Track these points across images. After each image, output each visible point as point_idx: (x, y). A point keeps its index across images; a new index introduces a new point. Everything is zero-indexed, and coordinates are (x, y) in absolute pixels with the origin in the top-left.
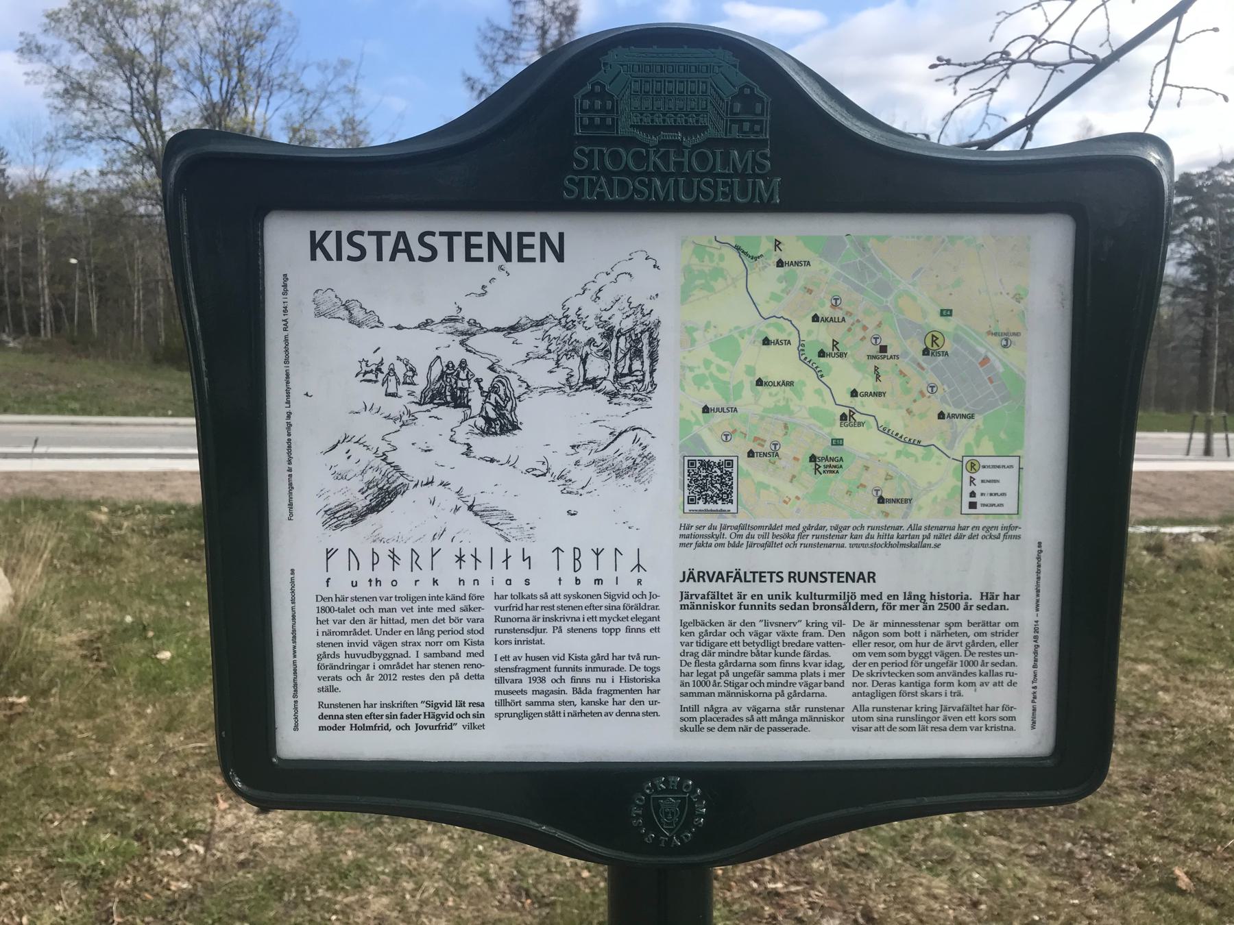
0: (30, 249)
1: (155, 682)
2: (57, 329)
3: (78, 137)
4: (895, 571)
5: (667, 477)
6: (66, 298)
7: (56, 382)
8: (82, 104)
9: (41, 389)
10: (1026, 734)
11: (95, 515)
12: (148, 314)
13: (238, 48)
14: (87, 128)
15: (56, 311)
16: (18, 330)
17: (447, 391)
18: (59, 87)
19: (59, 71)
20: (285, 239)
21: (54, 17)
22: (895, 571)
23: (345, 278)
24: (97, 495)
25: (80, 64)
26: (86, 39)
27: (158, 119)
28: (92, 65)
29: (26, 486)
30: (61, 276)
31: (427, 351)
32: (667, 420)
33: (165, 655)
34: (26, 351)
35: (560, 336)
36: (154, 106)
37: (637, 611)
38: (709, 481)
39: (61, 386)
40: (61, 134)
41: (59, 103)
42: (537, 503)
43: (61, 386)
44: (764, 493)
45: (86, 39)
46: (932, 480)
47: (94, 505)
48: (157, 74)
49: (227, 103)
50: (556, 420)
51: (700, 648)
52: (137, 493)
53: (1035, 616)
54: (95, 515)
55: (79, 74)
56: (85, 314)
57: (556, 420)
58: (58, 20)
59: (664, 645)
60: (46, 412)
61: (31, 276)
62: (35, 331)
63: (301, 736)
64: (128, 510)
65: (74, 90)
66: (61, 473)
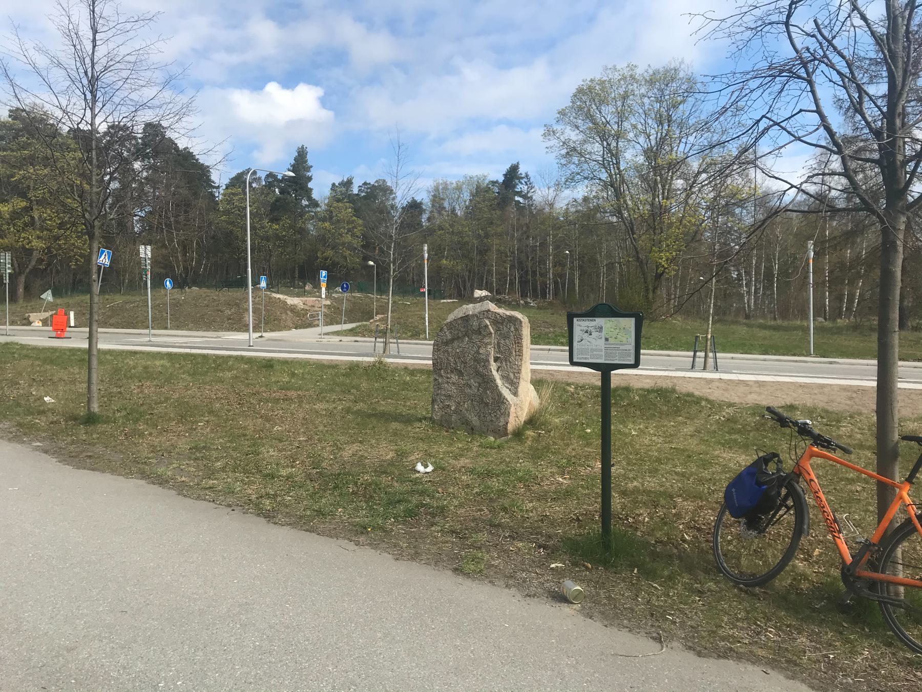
0: (543, 245)
1: (583, 436)
2: (556, 294)
3: (571, 180)
4: (622, 347)
5: (603, 339)
6: (562, 276)
7: (554, 327)
8: (575, 159)
9: (547, 330)
10: (633, 362)
11: (568, 388)
12: (609, 282)
13: (669, 110)
14: (578, 174)
15: (556, 283)
16: (535, 297)
17: (587, 332)
18: (564, 152)
19: (564, 143)
20: (575, 320)
21: (562, 113)
22: (622, 347)
23: (579, 323)
24: (570, 381)
25: (574, 136)
26: (579, 122)
27: (618, 163)
28: (581, 137)
29: (541, 375)
30: (559, 263)
31: (585, 329)
32: (603, 334)
33: (589, 431)
34: (539, 308)
35: (595, 327)
36: (616, 155)
37: (601, 350)
38: (607, 339)
39: (557, 329)
40: (563, 180)
41: (563, 161)
42: (593, 341)
43: (557, 329)
44: (611, 341)
45: (579, 122)
46: (624, 340)
47: (569, 385)
48: (618, 136)
49: (662, 141)
50: (595, 334)
51: (606, 353)
52: (588, 381)
53: (633, 352)
54: (568, 388)
55: (574, 142)
56: (572, 282)
57: (595, 334)
58: (564, 115)
59: (603, 353)
60: (549, 344)
61: (543, 261)
62: (544, 296)
63: (575, 360)
64: (583, 387)
65: (572, 151)
66: (555, 371)
